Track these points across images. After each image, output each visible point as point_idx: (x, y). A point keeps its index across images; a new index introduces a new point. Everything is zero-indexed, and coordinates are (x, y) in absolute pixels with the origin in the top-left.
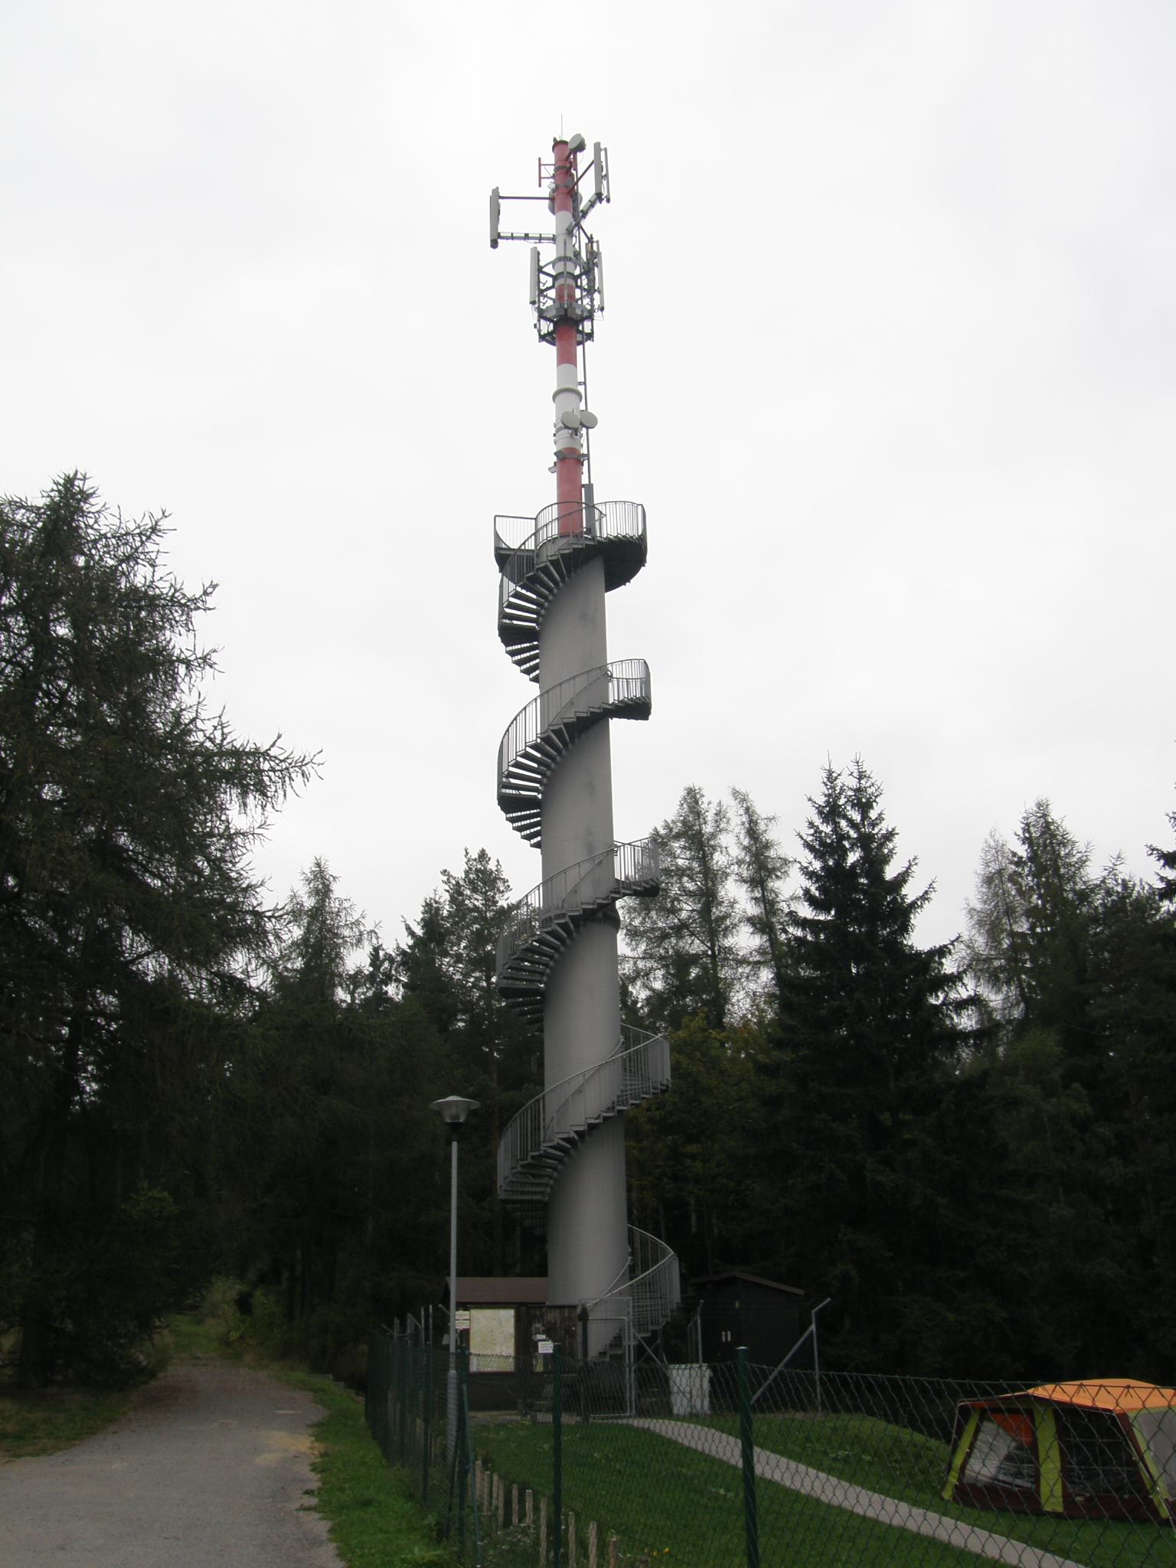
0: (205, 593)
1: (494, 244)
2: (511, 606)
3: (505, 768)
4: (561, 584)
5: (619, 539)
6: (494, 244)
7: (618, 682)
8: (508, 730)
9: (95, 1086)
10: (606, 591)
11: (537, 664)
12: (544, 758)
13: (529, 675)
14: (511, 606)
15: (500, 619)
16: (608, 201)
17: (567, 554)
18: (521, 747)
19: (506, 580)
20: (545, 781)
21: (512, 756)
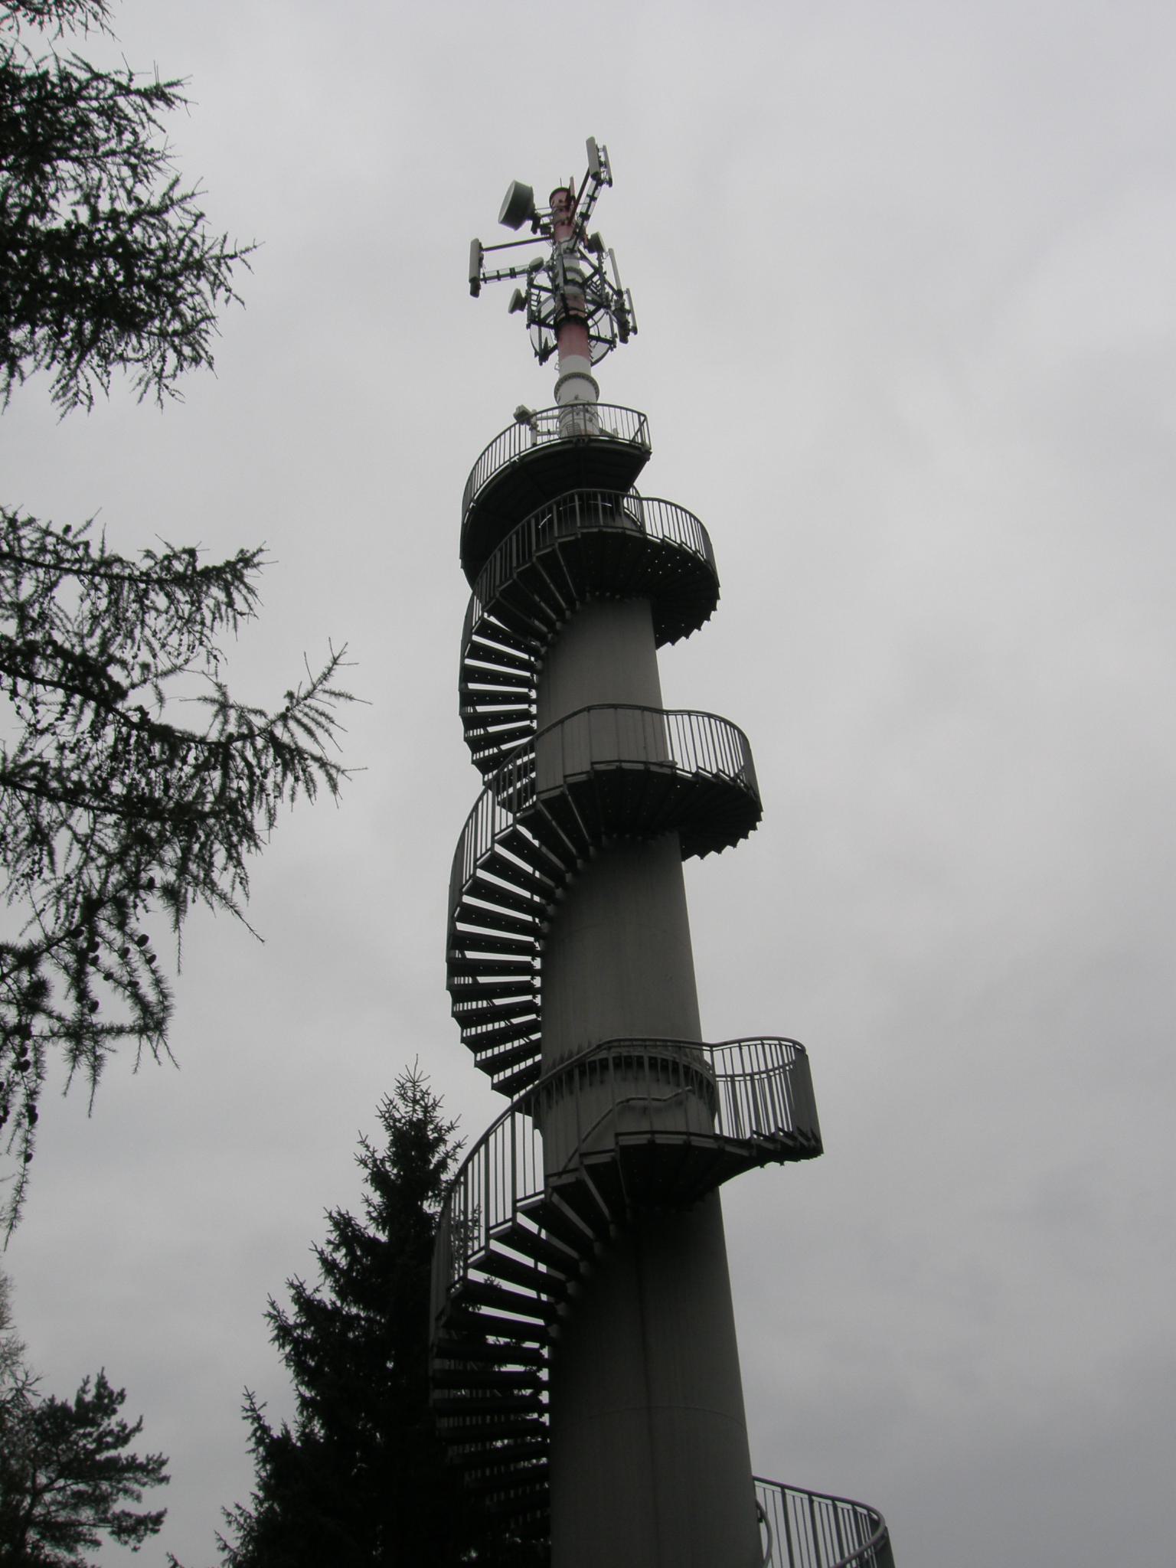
0: (23, 1176)
1: (475, 291)
2: (480, 889)
3: (468, 870)
4: (568, 613)
5: (704, 778)
6: (475, 291)
7: (752, 1080)
8: (475, 808)
9: (139, 263)
10: (684, 860)
11: (532, 762)
12: (557, 1243)
13: (510, 1095)
14: (480, 889)
15: (452, 921)
16: (610, 183)
17: (605, 1165)
18: (501, 1212)
19: (477, 602)
20: (561, 1309)
21: (484, 843)
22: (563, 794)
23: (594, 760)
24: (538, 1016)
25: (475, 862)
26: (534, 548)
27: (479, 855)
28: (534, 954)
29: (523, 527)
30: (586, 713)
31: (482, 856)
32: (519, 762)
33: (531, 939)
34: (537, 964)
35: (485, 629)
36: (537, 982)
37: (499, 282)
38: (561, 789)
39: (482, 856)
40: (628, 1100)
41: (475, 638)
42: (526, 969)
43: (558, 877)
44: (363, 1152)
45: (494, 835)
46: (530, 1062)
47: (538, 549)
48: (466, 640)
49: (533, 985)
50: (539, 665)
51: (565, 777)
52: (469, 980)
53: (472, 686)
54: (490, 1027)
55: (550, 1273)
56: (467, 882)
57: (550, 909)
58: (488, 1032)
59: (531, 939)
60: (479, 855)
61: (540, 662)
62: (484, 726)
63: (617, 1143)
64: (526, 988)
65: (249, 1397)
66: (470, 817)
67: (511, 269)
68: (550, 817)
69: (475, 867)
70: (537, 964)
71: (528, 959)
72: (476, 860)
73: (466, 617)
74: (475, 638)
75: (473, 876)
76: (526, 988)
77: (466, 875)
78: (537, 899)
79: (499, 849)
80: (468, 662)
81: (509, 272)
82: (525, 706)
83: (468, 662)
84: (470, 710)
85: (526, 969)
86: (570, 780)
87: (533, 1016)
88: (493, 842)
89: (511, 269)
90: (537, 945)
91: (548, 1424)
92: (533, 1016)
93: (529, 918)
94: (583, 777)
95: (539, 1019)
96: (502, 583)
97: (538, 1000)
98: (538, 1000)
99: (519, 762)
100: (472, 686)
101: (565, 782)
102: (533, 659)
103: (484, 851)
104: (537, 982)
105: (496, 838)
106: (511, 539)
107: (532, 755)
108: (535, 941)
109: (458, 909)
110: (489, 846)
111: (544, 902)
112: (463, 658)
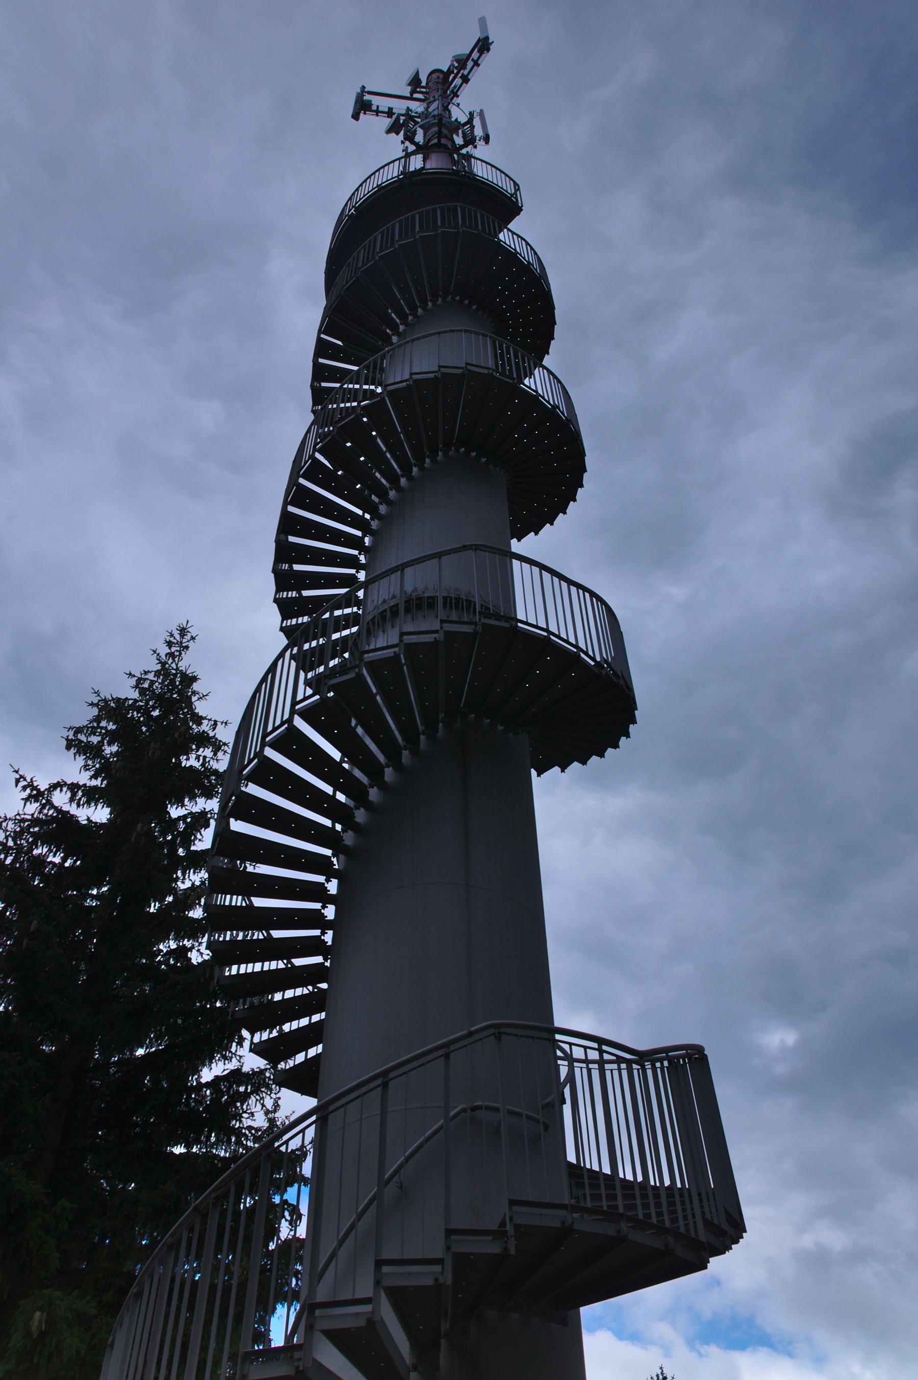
1: (356, 117)
6: (356, 117)
21: (280, 711)
22: (397, 656)
23: (441, 364)
24: (326, 959)
25: (264, 738)
26: (397, 238)
27: (270, 728)
28: (330, 874)
29: (388, 229)
30: (437, 335)
31: (275, 729)
32: (337, 613)
33: (328, 852)
34: (333, 887)
35: (315, 472)
36: (330, 912)
37: (375, 117)
38: (396, 649)
39: (275, 729)
40: (475, 1109)
41: (302, 481)
42: (316, 893)
43: (374, 770)
44: (195, 641)
45: (294, 703)
46: (304, 1022)
47: (400, 239)
48: (293, 481)
49: (323, 916)
50: (349, 839)
51: (411, 374)
52: (238, 901)
53: (321, 360)
54: (258, 967)
55: (348, 804)
56: (250, 761)
57: (360, 816)
58: (253, 973)
59: (328, 852)
60: (270, 728)
61: (350, 833)
62: (248, 893)
63: (448, 1248)
64: (314, 919)
65: (131, 675)
66: (264, 679)
67: (389, 108)
68: (384, 449)
69: (263, 745)
70: (333, 887)
71: (321, 879)
72: (266, 735)
73: (294, 462)
74: (302, 481)
75: (259, 754)
76: (314, 919)
77: (251, 752)
78: (341, 797)
79: (299, 722)
80: (291, 509)
81: (386, 110)
82: (321, 879)
83: (291, 509)
84: (286, 566)
85: (316, 893)
86: (415, 377)
87: (319, 959)
88: (293, 712)
89: (389, 108)
90: (335, 860)
91: (330, 943)
92: (319, 959)
93: (327, 823)
94: (431, 376)
95: (328, 964)
96: (364, 265)
97: (328, 937)
98: (328, 937)
99: (337, 613)
100: (321, 360)
101: (401, 641)
102: (338, 827)
103: (278, 723)
104: (330, 912)
105: (297, 707)
106: (375, 238)
107: (354, 629)
108: (334, 855)
109: (295, 487)
110: (286, 716)
111: (351, 803)
112: (285, 504)
